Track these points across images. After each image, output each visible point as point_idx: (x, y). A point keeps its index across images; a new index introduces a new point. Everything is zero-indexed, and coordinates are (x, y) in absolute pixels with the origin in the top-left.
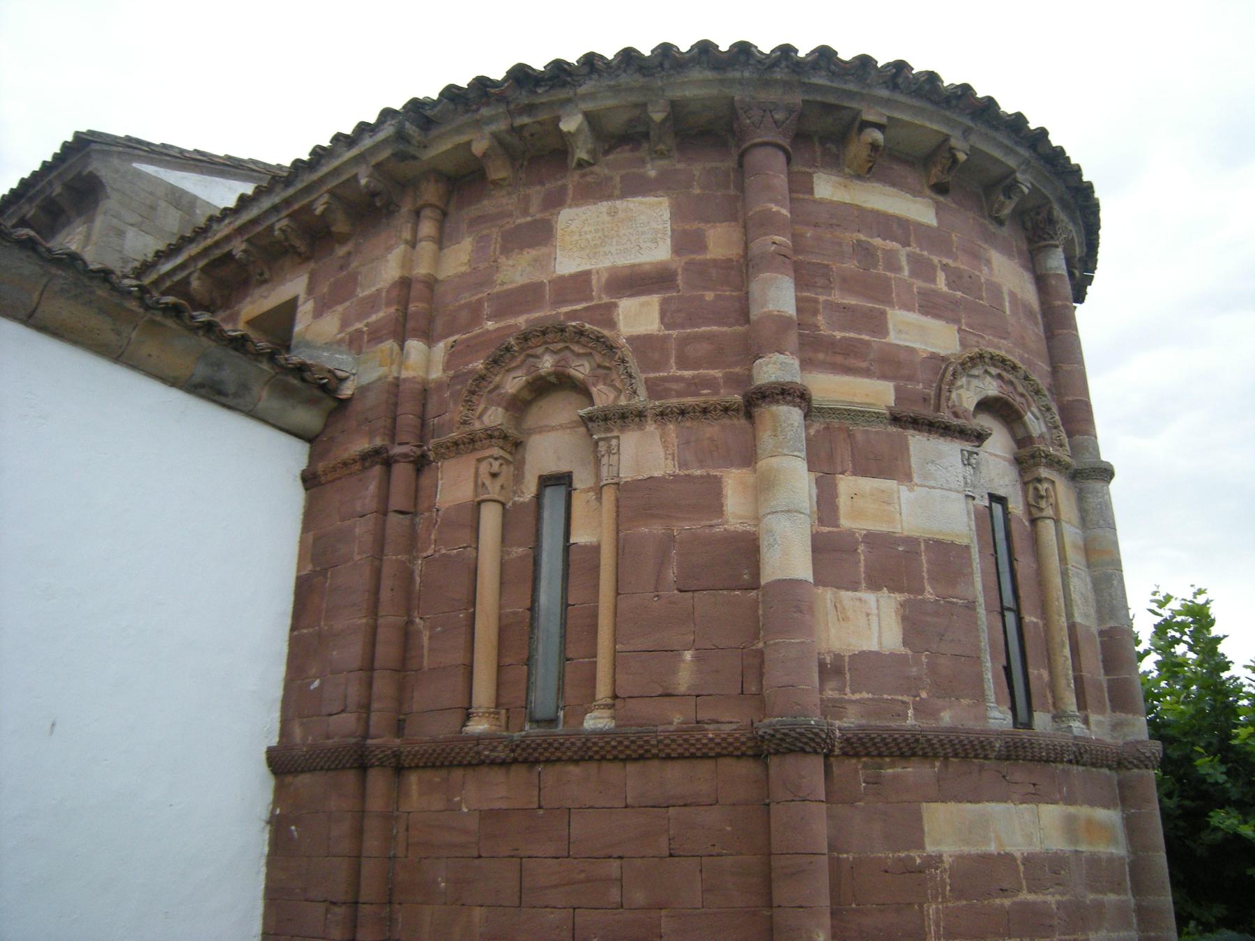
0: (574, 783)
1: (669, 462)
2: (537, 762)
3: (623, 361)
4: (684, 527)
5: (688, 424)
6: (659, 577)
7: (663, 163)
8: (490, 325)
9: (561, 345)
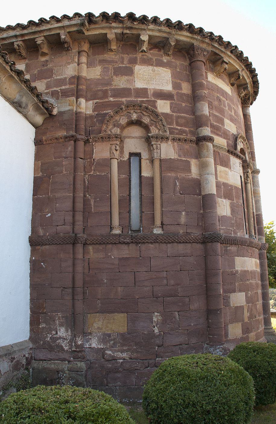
0: (151, 249)
1: (176, 154)
2: (140, 243)
3: (161, 120)
7: (169, 58)
8: (111, 99)
9: (139, 111)
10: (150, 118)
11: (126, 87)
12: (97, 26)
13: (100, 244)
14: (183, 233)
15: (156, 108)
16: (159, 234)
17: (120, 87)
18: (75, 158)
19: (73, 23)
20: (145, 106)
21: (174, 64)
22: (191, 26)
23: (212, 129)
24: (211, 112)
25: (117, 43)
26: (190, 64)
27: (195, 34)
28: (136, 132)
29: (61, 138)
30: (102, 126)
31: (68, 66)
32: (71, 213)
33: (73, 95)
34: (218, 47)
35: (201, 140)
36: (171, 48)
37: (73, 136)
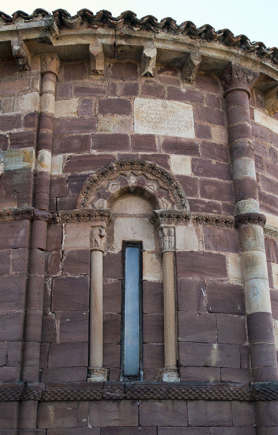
0: (158, 412)
1: (201, 244)
2: (138, 399)
3: (177, 188)
4: (209, 279)
5: (209, 226)
6: (199, 305)
7: (188, 85)
8: (94, 152)
9: (140, 172)
10: (158, 183)
11: (118, 132)
12: (72, 32)
13: (69, 400)
14: (215, 381)
15: (168, 167)
16: (173, 384)
17: (109, 133)
18: (31, 248)
19: (33, 26)
20: (151, 164)
21: (198, 96)
22: (226, 33)
23: (262, 202)
24: (260, 173)
25: (105, 61)
26: (225, 96)
27: (234, 46)
28: (135, 206)
29: (8, 214)
30: (78, 197)
31: (24, 96)
32: (20, 344)
33: (30, 144)
34: (272, 67)
35: (243, 221)
36: (194, 69)
37: (28, 212)
